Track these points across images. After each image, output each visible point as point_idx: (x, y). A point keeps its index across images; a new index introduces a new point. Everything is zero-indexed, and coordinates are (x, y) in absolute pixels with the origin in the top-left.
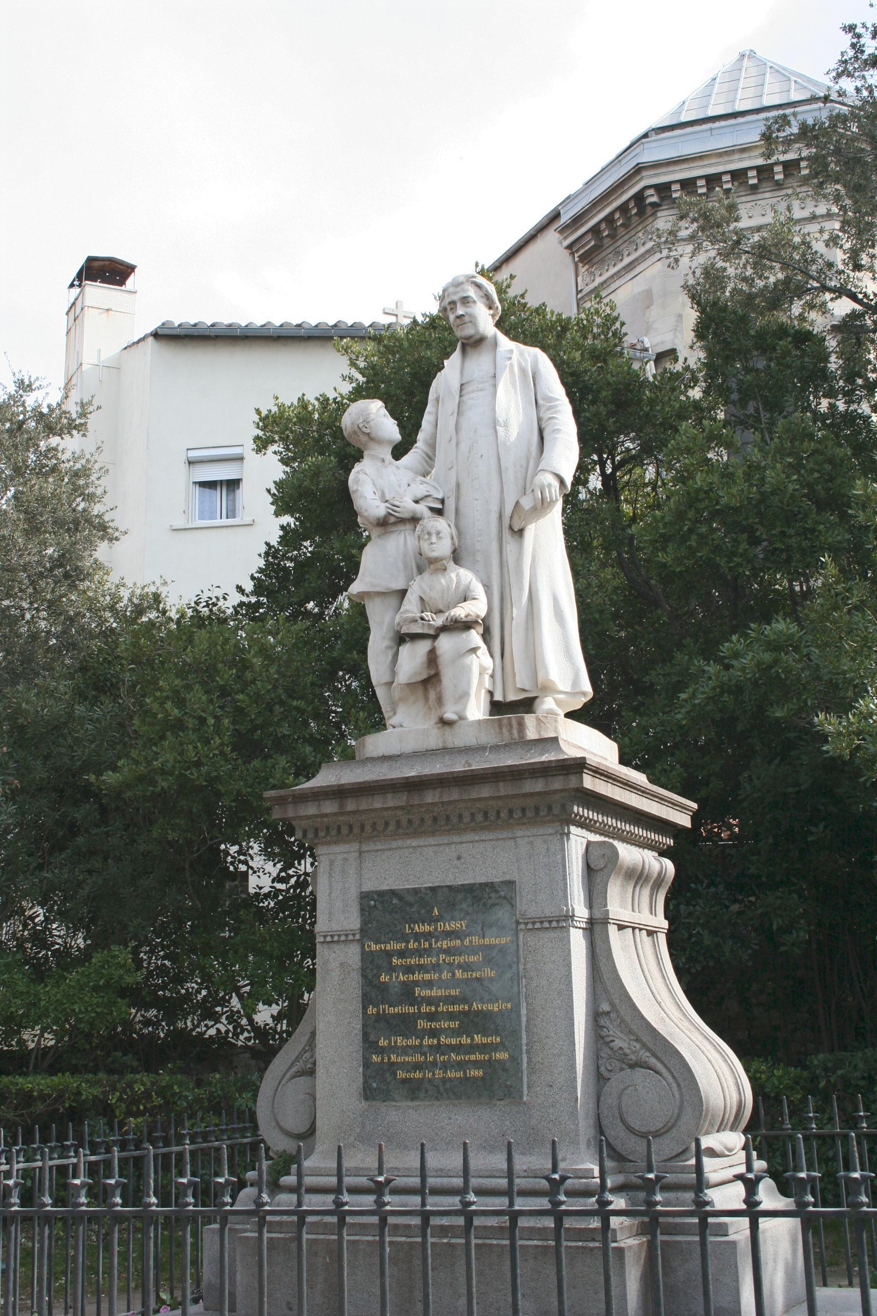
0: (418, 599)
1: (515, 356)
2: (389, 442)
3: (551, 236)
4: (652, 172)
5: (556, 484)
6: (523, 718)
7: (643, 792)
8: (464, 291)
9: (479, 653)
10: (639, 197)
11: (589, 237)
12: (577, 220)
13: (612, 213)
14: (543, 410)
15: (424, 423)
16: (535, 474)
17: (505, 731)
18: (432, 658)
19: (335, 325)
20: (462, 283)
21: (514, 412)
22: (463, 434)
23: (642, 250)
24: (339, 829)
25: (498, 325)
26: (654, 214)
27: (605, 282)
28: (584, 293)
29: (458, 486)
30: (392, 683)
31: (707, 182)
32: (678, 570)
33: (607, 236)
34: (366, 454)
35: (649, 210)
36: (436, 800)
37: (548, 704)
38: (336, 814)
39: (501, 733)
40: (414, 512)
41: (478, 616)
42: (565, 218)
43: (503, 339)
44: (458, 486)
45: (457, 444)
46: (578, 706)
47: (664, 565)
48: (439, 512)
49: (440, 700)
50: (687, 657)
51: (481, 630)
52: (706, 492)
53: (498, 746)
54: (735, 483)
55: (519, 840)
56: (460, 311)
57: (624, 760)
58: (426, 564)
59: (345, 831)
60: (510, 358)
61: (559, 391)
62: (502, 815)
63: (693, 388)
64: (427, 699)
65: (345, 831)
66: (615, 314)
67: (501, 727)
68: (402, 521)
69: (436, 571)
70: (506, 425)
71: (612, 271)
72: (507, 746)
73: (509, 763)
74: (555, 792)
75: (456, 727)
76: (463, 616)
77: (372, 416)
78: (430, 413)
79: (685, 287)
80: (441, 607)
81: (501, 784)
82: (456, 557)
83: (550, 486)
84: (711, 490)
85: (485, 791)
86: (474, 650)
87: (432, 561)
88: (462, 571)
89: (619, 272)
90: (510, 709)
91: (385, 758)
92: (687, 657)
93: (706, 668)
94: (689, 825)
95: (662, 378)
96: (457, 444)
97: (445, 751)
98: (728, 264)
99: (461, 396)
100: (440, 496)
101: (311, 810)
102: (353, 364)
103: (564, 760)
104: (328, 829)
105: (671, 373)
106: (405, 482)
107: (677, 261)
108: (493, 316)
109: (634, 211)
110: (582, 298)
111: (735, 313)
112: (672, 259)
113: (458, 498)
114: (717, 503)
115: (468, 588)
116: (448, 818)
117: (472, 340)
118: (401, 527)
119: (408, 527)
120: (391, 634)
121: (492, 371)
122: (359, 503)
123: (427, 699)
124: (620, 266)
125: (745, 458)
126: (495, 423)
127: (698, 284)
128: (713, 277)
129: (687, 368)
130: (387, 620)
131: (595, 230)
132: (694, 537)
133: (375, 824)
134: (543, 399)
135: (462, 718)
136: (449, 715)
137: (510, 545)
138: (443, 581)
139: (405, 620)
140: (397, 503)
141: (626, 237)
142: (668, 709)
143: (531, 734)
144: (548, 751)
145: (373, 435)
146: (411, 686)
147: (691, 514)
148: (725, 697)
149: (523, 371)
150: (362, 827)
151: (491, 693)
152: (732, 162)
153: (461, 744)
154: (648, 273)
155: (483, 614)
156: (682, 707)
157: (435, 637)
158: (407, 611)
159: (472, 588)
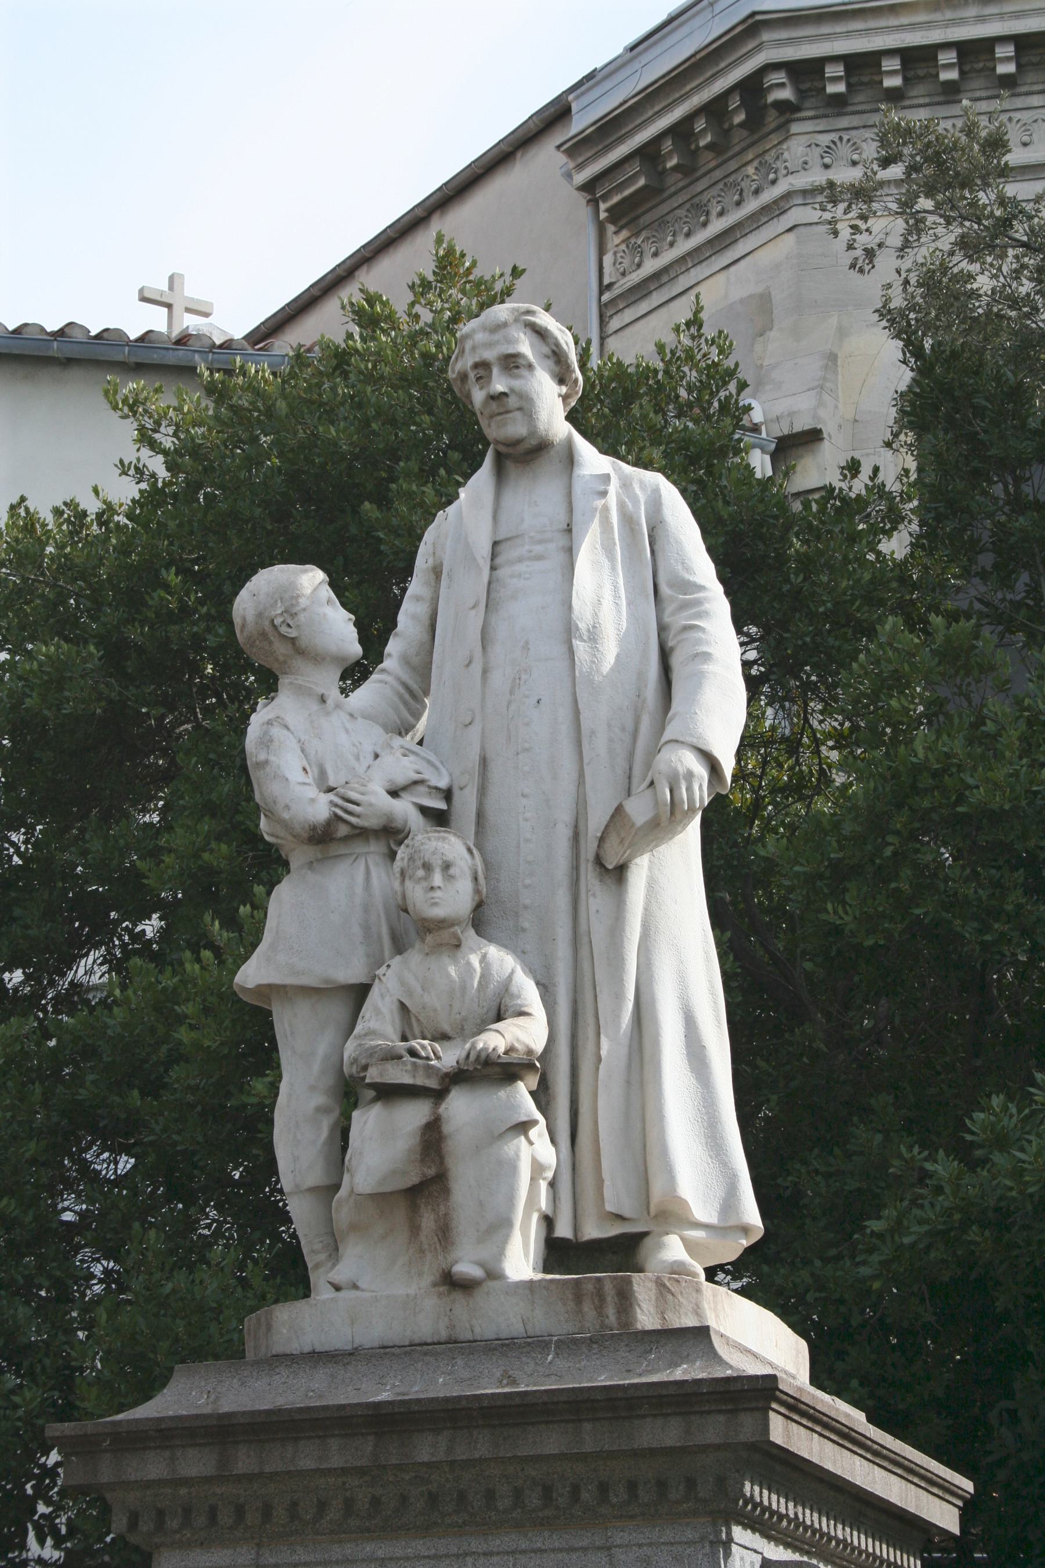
0: (395, 1007)
1: (613, 489)
2: (337, 659)
3: (547, 158)
4: (783, 34)
5: (701, 772)
6: (628, 1282)
7: (876, 1454)
8: (510, 341)
9: (533, 1133)
10: (752, 87)
11: (635, 167)
12: (609, 128)
13: (689, 119)
14: (669, 609)
15: (401, 618)
16: (655, 750)
17: (588, 1307)
18: (433, 1139)
19: (61, 332)
20: (505, 325)
21: (602, 605)
22: (498, 651)
23: (752, 205)
24: (213, 1514)
25: (572, 417)
26: (784, 126)
27: (665, 270)
28: (616, 291)
29: (484, 762)
30: (337, 1187)
31: (904, 64)
32: (869, 942)
33: (676, 168)
34: (284, 681)
35: (772, 119)
36: (441, 1455)
37: (673, 1249)
38: (207, 1480)
39: (580, 1311)
40: (390, 817)
41: (530, 1052)
42: (581, 122)
43: (584, 448)
44: (484, 762)
45: (485, 672)
46: (733, 1257)
47: (837, 931)
48: (439, 818)
49: (445, 1234)
50: (879, 1137)
51: (533, 1081)
52: (935, 774)
53: (575, 1342)
54: (999, 756)
55: (619, 1555)
56: (499, 386)
57: (816, 1380)
58: (411, 931)
59: (225, 1518)
60: (604, 494)
61: (703, 568)
62: (585, 1496)
63: (888, 534)
64: (415, 1230)
65: (225, 1518)
66: (730, 363)
67: (578, 1299)
68: (362, 834)
69: (438, 948)
70: (593, 637)
71: (684, 246)
72: (599, 1342)
73: (603, 1380)
74: (705, 1448)
75: (479, 1294)
76: (501, 1050)
77: (303, 602)
78: (418, 599)
79: (884, 312)
80: (446, 1028)
81: (587, 1426)
82: (480, 919)
83: (690, 775)
84: (945, 770)
85: (551, 1441)
86: (524, 1127)
87: (429, 927)
88: (493, 951)
89: (698, 249)
90: (596, 1257)
91: (317, 1358)
92: (879, 1137)
93: (929, 1166)
94: (956, 1530)
95: (822, 510)
96: (485, 672)
97: (453, 1346)
98: (975, 268)
99: (493, 568)
100: (443, 784)
101: (153, 1467)
102: (146, 439)
103: (728, 1379)
104: (187, 1511)
105: (844, 500)
106: (368, 748)
107: (870, 254)
108: (565, 398)
109: (740, 118)
110: (613, 301)
111: (998, 378)
112: (859, 252)
113: (482, 791)
114: (961, 799)
115: (506, 986)
116: (462, 1497)
117: (521, 448)
118: (359, 847)
119: (376, 848)
120: (329, 1080)
121: (562, 518)
122: (266, 789)
123: (415, 1230)
124: (700, 237)
125: (1018, 702)
126: (569, 630)
127: (912, 308)
128: (940, 288)
129: (879, 491)
130: (323, 1048)
131: (648, 153)
132: (906, 872)
133: (294, 1504)
134: (671, 585)
135: (494, 1274)
136: (466, 1268)
137: (596, 898)
138: (452, 970)
139: (372, 1052)
140: (353, 795)
141: (718, 174)
142: (833, 1252)
143: (646, 1319)
144: (686, 1359)
145: (303, 643)
146: (380, 1199)
147: (899, 822)
148: (974, 1234)
149: (628, 521)
150: (267, 1512)
151: (548, 1221)
152: (962, 22)
153: (489, 1334)
154: (764, 257)
155: (539, 1045)
156: (871, 1251)
157: (439, 1095)
158: (370, 1033)
159: (514, 989)
